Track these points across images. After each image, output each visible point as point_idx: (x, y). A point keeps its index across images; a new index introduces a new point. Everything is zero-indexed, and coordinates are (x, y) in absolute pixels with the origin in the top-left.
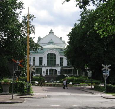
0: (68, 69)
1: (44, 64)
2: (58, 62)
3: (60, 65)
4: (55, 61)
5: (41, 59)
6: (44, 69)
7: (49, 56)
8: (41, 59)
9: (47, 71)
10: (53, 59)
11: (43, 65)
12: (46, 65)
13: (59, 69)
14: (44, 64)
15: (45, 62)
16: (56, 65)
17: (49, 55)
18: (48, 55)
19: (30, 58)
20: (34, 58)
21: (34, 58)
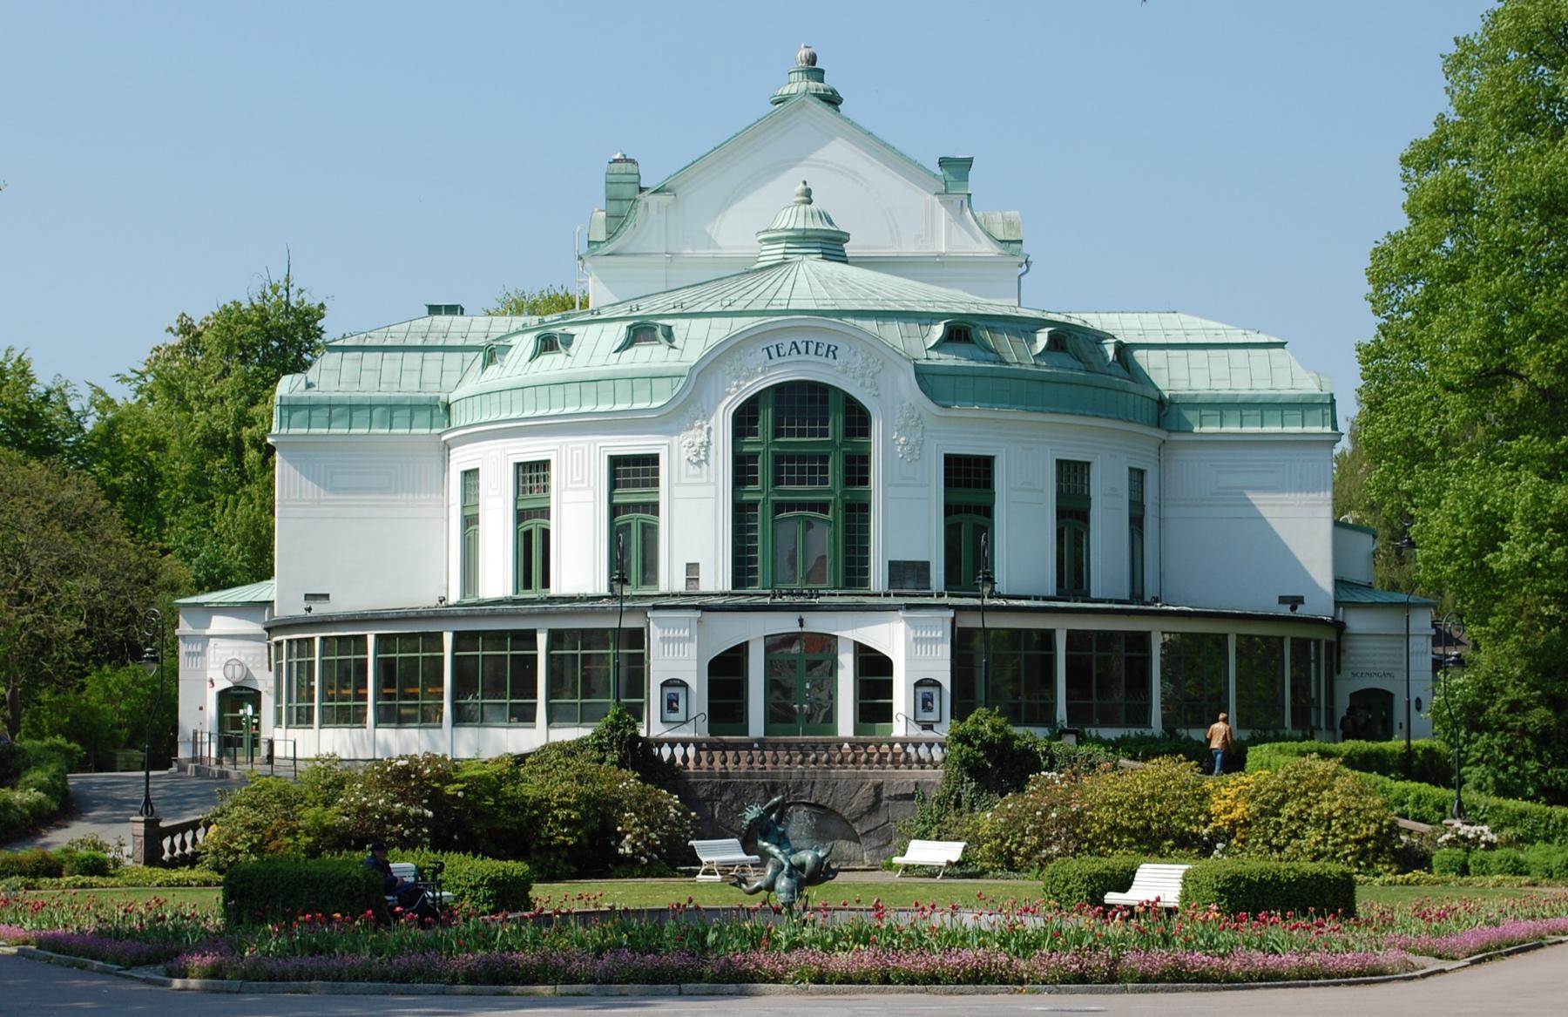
0: (1072, 635)
1: (692, 568)
2: (904, 518)
5: (632, 473)
6: (676, 655)
7: (761, 443)
9: (726, 671)
11: (671, 578)
12: (717, 577)
13: (913, 647)
14: (692, 568)
15: (696, 532)
16: (878, 577)
17: (766, 418)
18: (744, 419)
19: (470, 475)
20: (532, 474)
21: (532, 474)
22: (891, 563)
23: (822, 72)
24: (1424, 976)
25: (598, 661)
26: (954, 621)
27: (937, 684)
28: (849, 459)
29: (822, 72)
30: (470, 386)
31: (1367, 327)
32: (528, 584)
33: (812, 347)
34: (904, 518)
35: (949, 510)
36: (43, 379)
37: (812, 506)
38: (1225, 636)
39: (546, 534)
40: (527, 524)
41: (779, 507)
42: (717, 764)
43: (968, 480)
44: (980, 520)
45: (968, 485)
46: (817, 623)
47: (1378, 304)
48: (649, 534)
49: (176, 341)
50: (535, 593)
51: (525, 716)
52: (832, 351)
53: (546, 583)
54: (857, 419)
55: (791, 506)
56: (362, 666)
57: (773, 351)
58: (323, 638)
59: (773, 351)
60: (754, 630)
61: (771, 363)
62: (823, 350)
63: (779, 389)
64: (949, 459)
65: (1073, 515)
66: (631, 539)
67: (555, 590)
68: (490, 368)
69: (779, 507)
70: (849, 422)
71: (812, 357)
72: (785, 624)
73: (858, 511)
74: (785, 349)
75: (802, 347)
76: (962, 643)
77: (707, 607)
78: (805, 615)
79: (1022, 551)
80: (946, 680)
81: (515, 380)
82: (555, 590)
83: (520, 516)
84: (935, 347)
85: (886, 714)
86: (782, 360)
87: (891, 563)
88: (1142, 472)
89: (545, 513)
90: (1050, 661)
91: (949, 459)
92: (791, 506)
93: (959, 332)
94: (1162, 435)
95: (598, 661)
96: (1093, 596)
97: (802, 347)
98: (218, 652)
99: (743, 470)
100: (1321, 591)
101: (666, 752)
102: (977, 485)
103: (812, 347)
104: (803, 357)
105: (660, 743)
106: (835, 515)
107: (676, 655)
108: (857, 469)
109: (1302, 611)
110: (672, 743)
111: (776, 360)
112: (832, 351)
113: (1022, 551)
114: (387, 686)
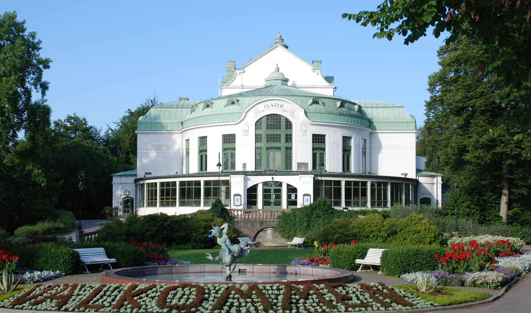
1: (244, 165)
2: (302, 152)
3: (310, 168)
4: (291, 148)
5: (229, 140)
6: (238, 186)
7: (263, 131)
8: (229, 140)
9: (251, 192)
10: (283, 144)
11: (239, 167)
12: (251, 167)
13: (305, 186)
14: (244, 165)
15: (245, 155)
16: (294, 168)
18: (258, 124)
20: (203, 140)
21: (203, 140)
22: (298, 163)
24: (494, 300)
25: (215, 190)
26: (314, 178)
28: (287, 135)
30: (188, 117)
31: (427, 96)
32: (202, 169)
33: (277, 105)
34: (302, 152)
35: (313, 149)
36: (89, 124)
37: (277, 148)
39: (206, 156)
40: (202, 154)
41: (268, 148)
42: (247, 217)
43: (318, 140)
44: (322, 151)
46: (277, 178)
47: (431, 90)
48: (233, 156)
49: (127, 114)
51: (198, 204)
53: (206, 169)
54: (289, 125)
55: (271, 148)
56: (156, 190)
57: (266, 106)
59: (266, 106)
60: (258, 180)
63: (267, 116)
64: (313, 135)
65: (346, 151)
67: (208, 171)
68: (193, 113)
69: (268, 148)
70: (287, 125)
71: (276, 107)
72: (268, 179)
73: (289, 149)
75: (274, 105)
76: (317, 184)
77: (245, 173)
78: (273, 177)
79: (333, 163)
80: (312, 194)
81: (198, 115)
82: (208, 171)
83: (200, 151)
84: (311, 105)
85: (255, 203)
87: (298, 163)
88: (365, 140)
89: (206, 151)
91: (313, 135)
92: (271, 148)
94: (371, 130)
95: (215, 190)
97: (274, 105)
98: (121, 189)
99: (258, 138)
100: (452, 62)
101: (236, 213)
102: (321, 142)
103: (277, 105)
104: (274, 107)
105: (234, 210)
106: (283, 149)
107: (238, 186)
108: (289, 138)
109: (407, 177)
110: (238, 211)
111: (267, 108)
112: (282, 106)
113: (333, 163)
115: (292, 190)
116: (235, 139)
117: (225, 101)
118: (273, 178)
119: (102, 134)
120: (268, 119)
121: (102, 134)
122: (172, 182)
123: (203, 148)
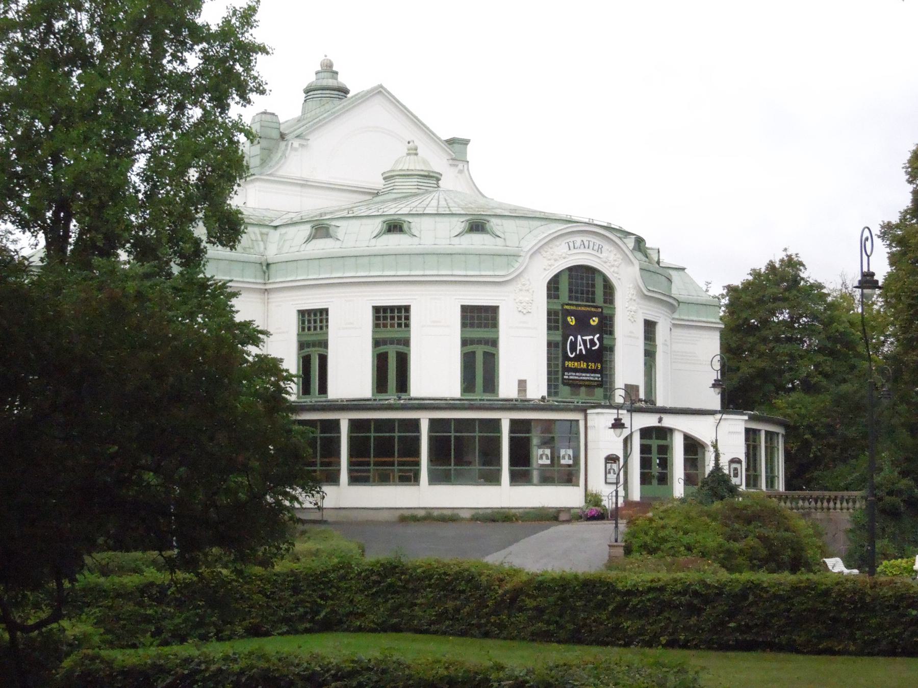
1: (522, 384)
5: (480, 321)
11: (507, 389)
14: (522, 384)
18: (553, 286)
23: (337, 73)
27: (739, 462)
29: (337, 73)
35: (465, 342)
38: (760, 430)
39: (323, 360)
43: (391, 321)
45: (479, 326)
48: (491, 360)
50: (314, 398)
52: (600, 249)
53: (323, 389)
57: (571, 245)
58: (513, 422)
59: (571, 245)
61: (570, 252)
62: (596, 248)
63: (571, 269)
66: (391, 366)
74: (578, 244)
78: (662, 416)
80: (743, 457)
85: (664, 479)
86: (576, 251)
90: (498, 441)
93: (395, 227)
96: (660, 403)
97: (586, 244)
102: (486, 326)
104: (590, 251)
114: (491, 455)
115: (693, 447)
116: (549, 321)
117: (306, 230)
118: (660, 420)
119: (740, 286)
120: (570, 277)
121: (740, 286)
122: (455, 420)
123: (311, 337)
